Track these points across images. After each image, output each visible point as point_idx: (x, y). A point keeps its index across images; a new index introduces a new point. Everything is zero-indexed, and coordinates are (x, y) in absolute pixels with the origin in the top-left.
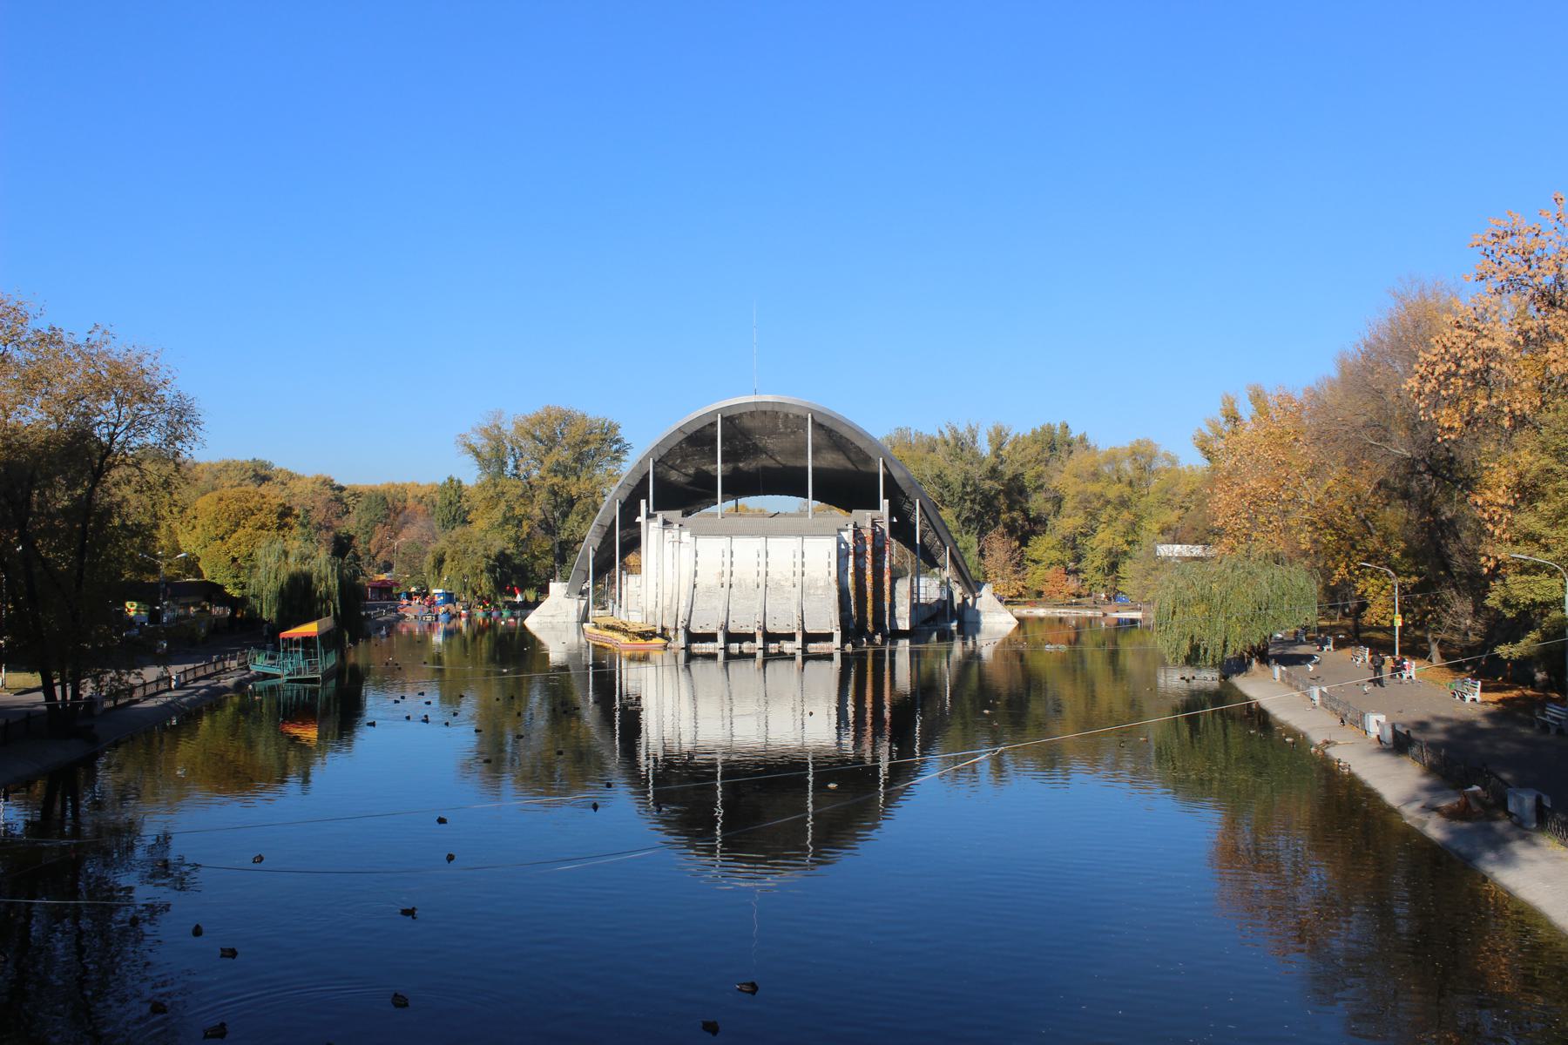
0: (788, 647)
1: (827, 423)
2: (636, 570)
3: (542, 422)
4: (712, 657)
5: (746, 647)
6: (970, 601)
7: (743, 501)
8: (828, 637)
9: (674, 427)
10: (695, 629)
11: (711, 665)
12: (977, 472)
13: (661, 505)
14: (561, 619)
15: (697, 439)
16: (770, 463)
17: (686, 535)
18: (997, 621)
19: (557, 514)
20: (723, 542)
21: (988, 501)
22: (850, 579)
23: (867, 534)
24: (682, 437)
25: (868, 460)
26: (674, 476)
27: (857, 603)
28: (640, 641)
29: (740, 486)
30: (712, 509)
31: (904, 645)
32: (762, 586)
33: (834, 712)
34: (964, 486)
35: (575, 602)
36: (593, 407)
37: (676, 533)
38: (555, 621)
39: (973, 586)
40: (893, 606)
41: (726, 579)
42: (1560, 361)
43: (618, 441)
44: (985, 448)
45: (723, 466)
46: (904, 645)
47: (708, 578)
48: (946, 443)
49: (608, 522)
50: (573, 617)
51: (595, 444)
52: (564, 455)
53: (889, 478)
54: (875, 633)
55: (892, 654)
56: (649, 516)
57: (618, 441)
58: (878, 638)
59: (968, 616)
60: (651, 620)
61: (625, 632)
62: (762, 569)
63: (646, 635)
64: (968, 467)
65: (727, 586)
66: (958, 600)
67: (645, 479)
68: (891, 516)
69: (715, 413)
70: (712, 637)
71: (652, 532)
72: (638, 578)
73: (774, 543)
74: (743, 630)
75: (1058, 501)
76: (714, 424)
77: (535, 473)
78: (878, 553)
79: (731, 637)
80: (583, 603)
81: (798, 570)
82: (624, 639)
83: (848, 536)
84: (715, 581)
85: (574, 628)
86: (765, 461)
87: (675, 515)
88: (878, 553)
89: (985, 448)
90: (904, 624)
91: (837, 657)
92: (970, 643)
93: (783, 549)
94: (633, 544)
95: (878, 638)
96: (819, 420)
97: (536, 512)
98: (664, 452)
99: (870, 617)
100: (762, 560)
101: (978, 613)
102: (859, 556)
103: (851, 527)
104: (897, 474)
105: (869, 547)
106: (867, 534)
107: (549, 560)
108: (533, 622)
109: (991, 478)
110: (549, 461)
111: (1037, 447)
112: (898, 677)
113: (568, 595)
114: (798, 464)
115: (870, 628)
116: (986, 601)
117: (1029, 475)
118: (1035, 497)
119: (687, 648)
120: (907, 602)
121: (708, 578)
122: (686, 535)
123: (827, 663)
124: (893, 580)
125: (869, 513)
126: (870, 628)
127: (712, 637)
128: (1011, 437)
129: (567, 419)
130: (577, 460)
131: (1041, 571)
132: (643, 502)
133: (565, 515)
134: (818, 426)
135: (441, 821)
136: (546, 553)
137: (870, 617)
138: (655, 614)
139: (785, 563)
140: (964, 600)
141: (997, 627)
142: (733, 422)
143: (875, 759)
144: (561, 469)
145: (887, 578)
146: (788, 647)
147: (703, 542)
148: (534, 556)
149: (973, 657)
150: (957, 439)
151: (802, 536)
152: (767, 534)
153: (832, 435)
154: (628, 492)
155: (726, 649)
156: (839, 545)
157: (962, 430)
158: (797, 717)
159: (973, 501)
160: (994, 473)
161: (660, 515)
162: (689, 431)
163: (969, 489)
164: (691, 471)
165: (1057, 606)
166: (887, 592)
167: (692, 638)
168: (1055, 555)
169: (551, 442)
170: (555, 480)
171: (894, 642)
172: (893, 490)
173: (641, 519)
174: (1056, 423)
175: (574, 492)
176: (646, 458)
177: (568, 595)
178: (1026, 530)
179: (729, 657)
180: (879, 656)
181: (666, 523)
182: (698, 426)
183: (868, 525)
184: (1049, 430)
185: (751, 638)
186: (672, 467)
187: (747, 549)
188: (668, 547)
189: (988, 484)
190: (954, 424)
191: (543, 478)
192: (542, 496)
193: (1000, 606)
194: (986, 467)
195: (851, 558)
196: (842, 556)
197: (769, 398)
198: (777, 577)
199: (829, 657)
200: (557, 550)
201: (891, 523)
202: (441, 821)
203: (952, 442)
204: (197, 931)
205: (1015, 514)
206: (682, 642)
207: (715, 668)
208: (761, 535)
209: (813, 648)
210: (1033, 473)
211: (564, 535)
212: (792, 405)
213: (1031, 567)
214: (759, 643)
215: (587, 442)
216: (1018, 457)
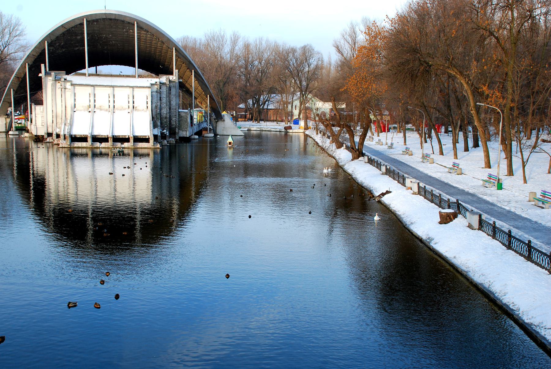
7: (99, 68)
29: (99, 58)
42: (504, 1)
45: (88, 46)
49: (22, 75)
56: (47, 74)
67: (43, 53)
69: (82, 18)
76: (82, 24)
80: (8, 120)
94: (37, 86)
98: (53, 38)
100: (111, 100)
112: (52, 158)
132: (43, 66)
135: (123, 175)
139: (116, 103)
143: (171, 204)
154: (33, 60)
158: (132, 183)
161: (53, 73)
162: (68, 27)
176: (42, 43)
188: (58, 91)
202: (123, 175)
204: (228, 276)
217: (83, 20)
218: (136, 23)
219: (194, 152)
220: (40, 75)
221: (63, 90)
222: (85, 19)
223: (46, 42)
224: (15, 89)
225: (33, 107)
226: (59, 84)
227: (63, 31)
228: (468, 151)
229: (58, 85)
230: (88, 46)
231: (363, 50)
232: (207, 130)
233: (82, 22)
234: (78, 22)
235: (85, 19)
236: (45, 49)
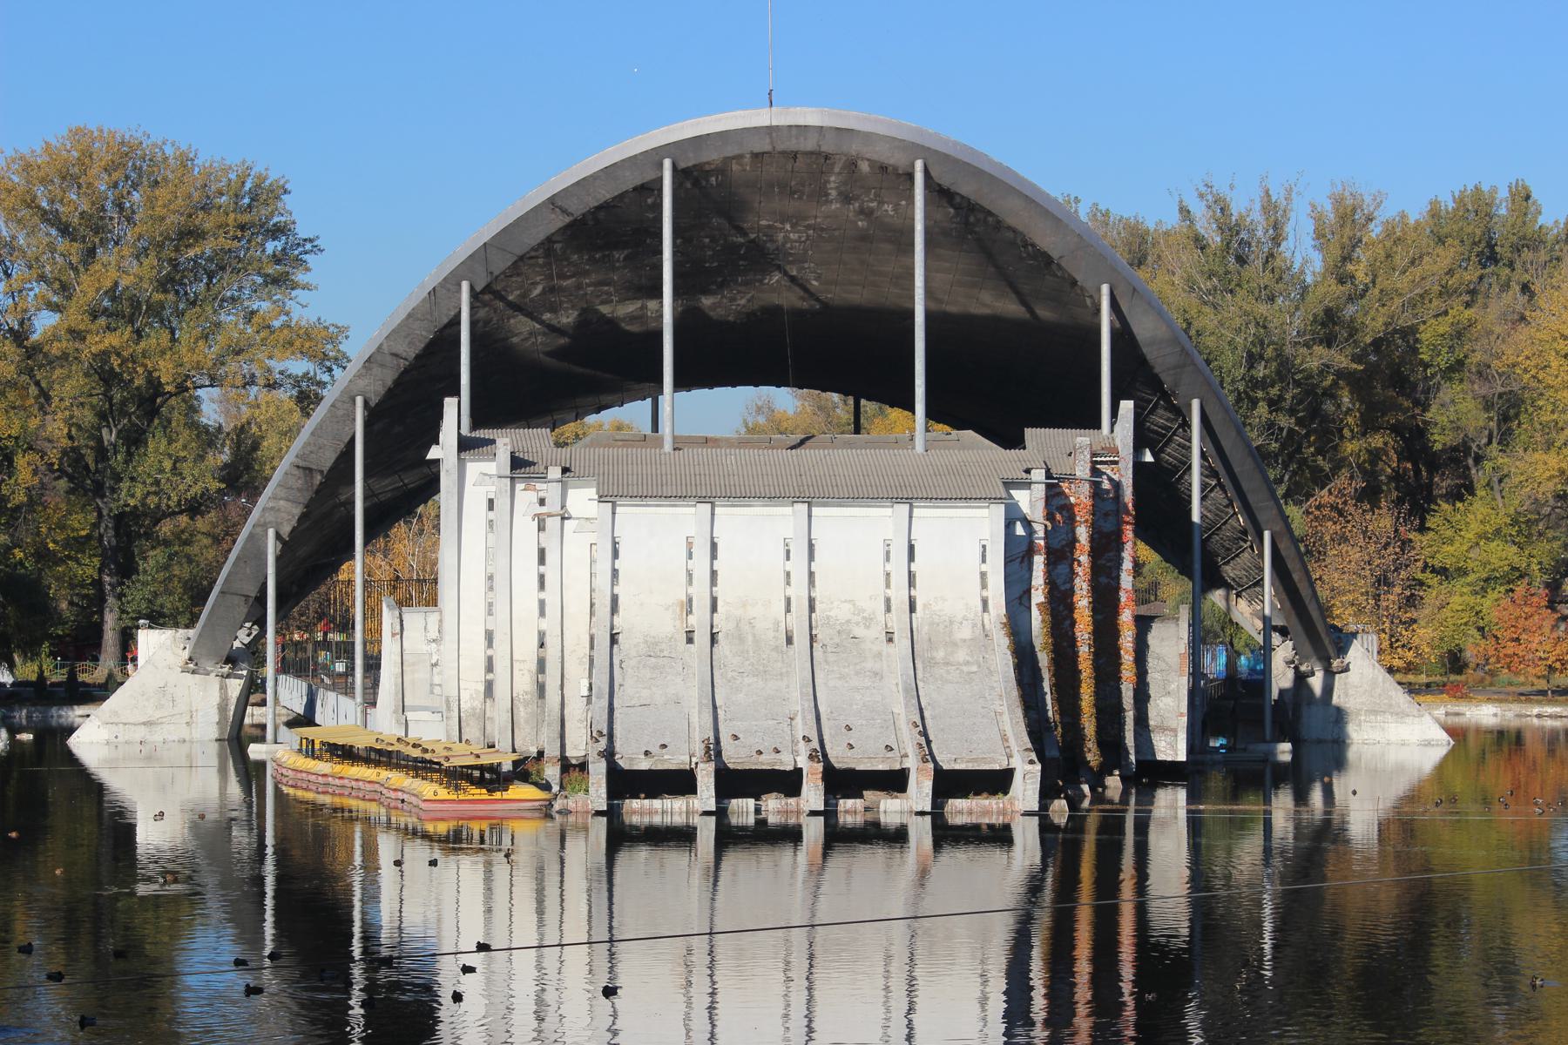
0: (891, 809)
1: (966, 188)
2: (420, 589)
3: (69, 178)
4: (683, 836)
5: (774, 806)
6: (1316, 682)
8: (998, 782)
9: (538, 195)
10: (633, 759)
11: (675, 859)
12: (1289, 321)
13: (491, 411)
14: (171, 732)
15: (603, 228)
16: (789, 299)
17: (582, 499)
18: (1394, 738)
19: (110, 436)
20: (687, 519)
21: (1312, 401)
22: (1037, 620)
23: (1079, 496)
24: (560, 221)
25: (1069, 290)
26: (522, 329)
27: (1057, 686)
28: (480, 793)
30: (635, 413)
31: (1172, 803)
32: (801, 640)
33: (998, 984)
34: (1252, 359)
35: (213, 682)
36: (209, 129)
37: (551, 491)
38: (157, 736)
39: (1325, 642)
40: (1142, 696)
41: (699, 620)
43: (277, 231)
44: (1304, 254)
45: (702, 293)
46: (1172, 803)
47: (649, 613)
48: (1199, 243)
49: (327, 459)
50: (208, 729)
51: (224, 242)
52: (123, 268)
53: (1123, 336)
54: (1106, 770)
55: (1142, 828)
56: (465, 445)
57: (277, 231)
58: (1114, 783)
59: (1312, 724)
60: (472, 732)
61: (423, 767)
62: (799, 591)
63: (491, 778)
64: (1263, 309)
65: (702, 638)
66: (1281, 678)
67: (445, 339)
68: (1138, 448)
69: (654, 157)
70: (681, 782)
71: (475, 489)
72: (433, 618)
73: (734, 521)
74: (766, 762)
75: (1508, 411)
76: (651, 189)
77: (44, 322)
78: (1106, 548)
79: (733, 783)
81: (899, 595)
82: (428, 789)
83: (1030, 501)
84: (669, 626)
85: (209, 754)
86: (775, 291)
87: (535, 440)
88: (1106, 548)
89: (1304, 254)
90: (1172, 746)
91: (1027, 835)
92: (1317, 797)
93: (855, 545)
95: (1114, 783)
96: (944, 178)
97: (56, 427)
99: (1089, 726)
100: (798, 566)
101: (1339, 717)
102: (1060, 555)
103: (1038, 475)
104: (1144, 328)
105: (1083, 533)
106: (1079, 496)
107: (87, 567)
108: (93, 737)
109: (1328, 342)
110: (88, 288)
111: (1446, 257)
112: (1155, 885)
113: (193, 665)
114: (888, 296)
115: (1093, 757)
116: (1361, 680)
117: (1431, 332)
118: (1448, 392)
119: (612, 813)
120: (1181, 684)
121: (649, 613)
122: (582, 499)
123: (996, 855)
124: (1143, 624)
125: (1082, 439)
126: (1093, 757)
127: (681, 782)
128: (1375, 230)
129: (134, 166)
130: (164, 285)
131: (1459, 596)
132: (450, 404)
133: (134, 440)
134: (938, 193)
136: (80, 544)
137: (1089, 726)
138: (483, 718)
140: (1301, 678)
141: (1393, 756)
142: (714, 188)
144: (122, 309)
145: (1126, 617)
146: (891, 809)
147: (636, 520)
148: (42, 555)
149: (1324, 837)
150: (1231, 230)
151: (909, 501)
152: (810, 499)
153: (977, 220)
155: (721, 813)
156: (1009, 525)
157: (1245, 204)
159: (1274, 404)
160: (1329, 326)
161: (505, 441)
162: (578, 208)
163: (1261, 371)
164: (567, 318)
165: (1526, 697)
166: (1127, 658)
167: (624, 783)
168: (1502, 554)
169: (88, 235)
170: (112, 340)
171: (1146, 797)
172: (1136, 375)
173: (444, 450)
174: (1497, 182)
175: (166, 372)
176: (451, 283)
177: (193, 665)
178: (1425, 478)
179: (729, 837)
180: (1111, 827)
181: (517, 463)
182: (605, 194)
183: (1082, 470)
184: (1476, 205)
185: (789, 783)
186: (516, 307)
187: (659, 536)
189: (1314, 359)
190: (1221, 187)
191: (77, 335)
192: (70, 386)
193: (1400, 697)
194: (1314, 306)
195: (1039, 561)
196: (1017, 556)
197: (809, 116)
198: (841, 612)
199: (1000, 836)
200: (109, 538)
201: (1139, 466)
203: (1215, 239)
205: (1377, 441)
206: (597, 793)
207: (681, 873)
208: (796, 499)
209: (962, 810)
210: (1444, 326)
211: (130, 495)
212: (868, 137)
213: (1434, 593)
214: (812, 795)
215: (196, 234)
216: (1401, 282)
217: (661, 165)
218: (919, 165)
219: (270, 840)
220: (433, 453)
221: (553, 524)
222: (667, 163)
223: (465, 286)
224: (286, 530)
225: (388, 618)
226: (532, 497)
227: (560, 224)
228: (1007, 828)
229: (526, 498)
230: (702, 293)
231: (113, 358)
232: (1260, 722)
233: (650, 176)
234: (631, 180)
235: (667, 163)
236: (455, 322)
